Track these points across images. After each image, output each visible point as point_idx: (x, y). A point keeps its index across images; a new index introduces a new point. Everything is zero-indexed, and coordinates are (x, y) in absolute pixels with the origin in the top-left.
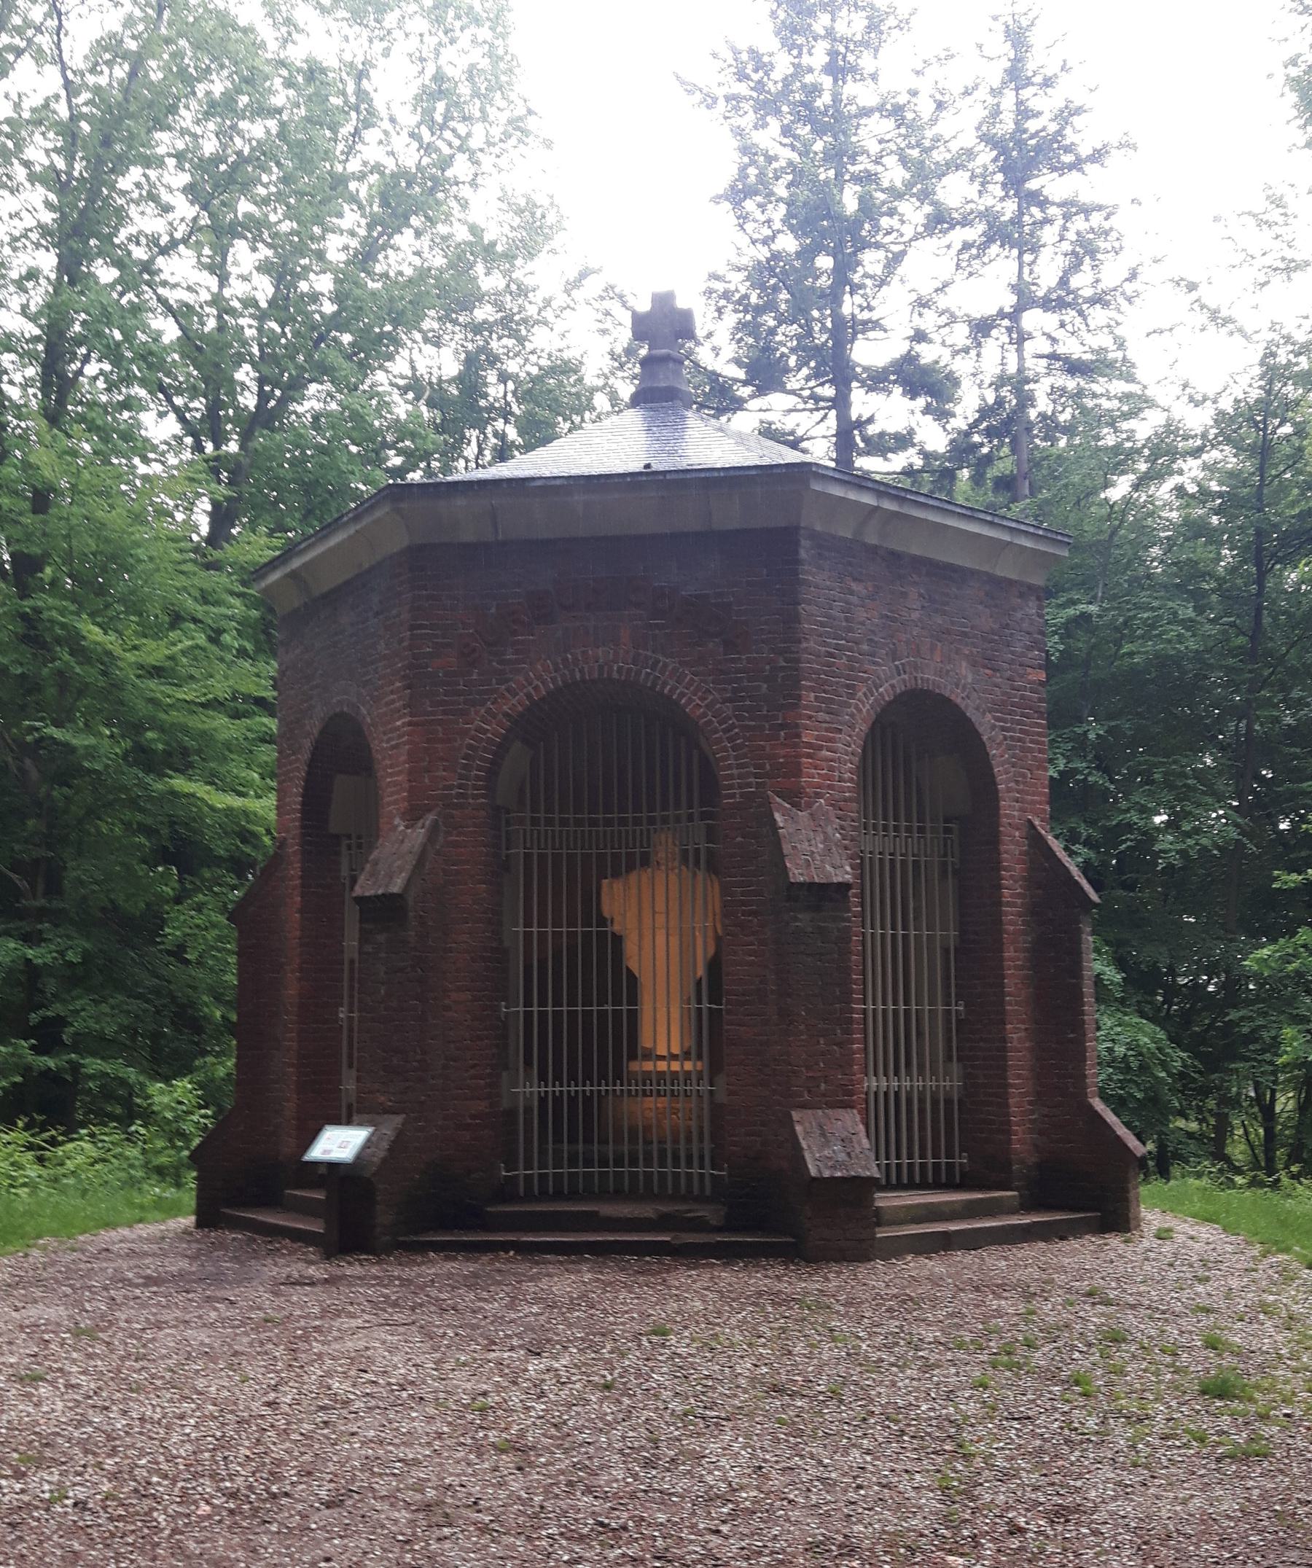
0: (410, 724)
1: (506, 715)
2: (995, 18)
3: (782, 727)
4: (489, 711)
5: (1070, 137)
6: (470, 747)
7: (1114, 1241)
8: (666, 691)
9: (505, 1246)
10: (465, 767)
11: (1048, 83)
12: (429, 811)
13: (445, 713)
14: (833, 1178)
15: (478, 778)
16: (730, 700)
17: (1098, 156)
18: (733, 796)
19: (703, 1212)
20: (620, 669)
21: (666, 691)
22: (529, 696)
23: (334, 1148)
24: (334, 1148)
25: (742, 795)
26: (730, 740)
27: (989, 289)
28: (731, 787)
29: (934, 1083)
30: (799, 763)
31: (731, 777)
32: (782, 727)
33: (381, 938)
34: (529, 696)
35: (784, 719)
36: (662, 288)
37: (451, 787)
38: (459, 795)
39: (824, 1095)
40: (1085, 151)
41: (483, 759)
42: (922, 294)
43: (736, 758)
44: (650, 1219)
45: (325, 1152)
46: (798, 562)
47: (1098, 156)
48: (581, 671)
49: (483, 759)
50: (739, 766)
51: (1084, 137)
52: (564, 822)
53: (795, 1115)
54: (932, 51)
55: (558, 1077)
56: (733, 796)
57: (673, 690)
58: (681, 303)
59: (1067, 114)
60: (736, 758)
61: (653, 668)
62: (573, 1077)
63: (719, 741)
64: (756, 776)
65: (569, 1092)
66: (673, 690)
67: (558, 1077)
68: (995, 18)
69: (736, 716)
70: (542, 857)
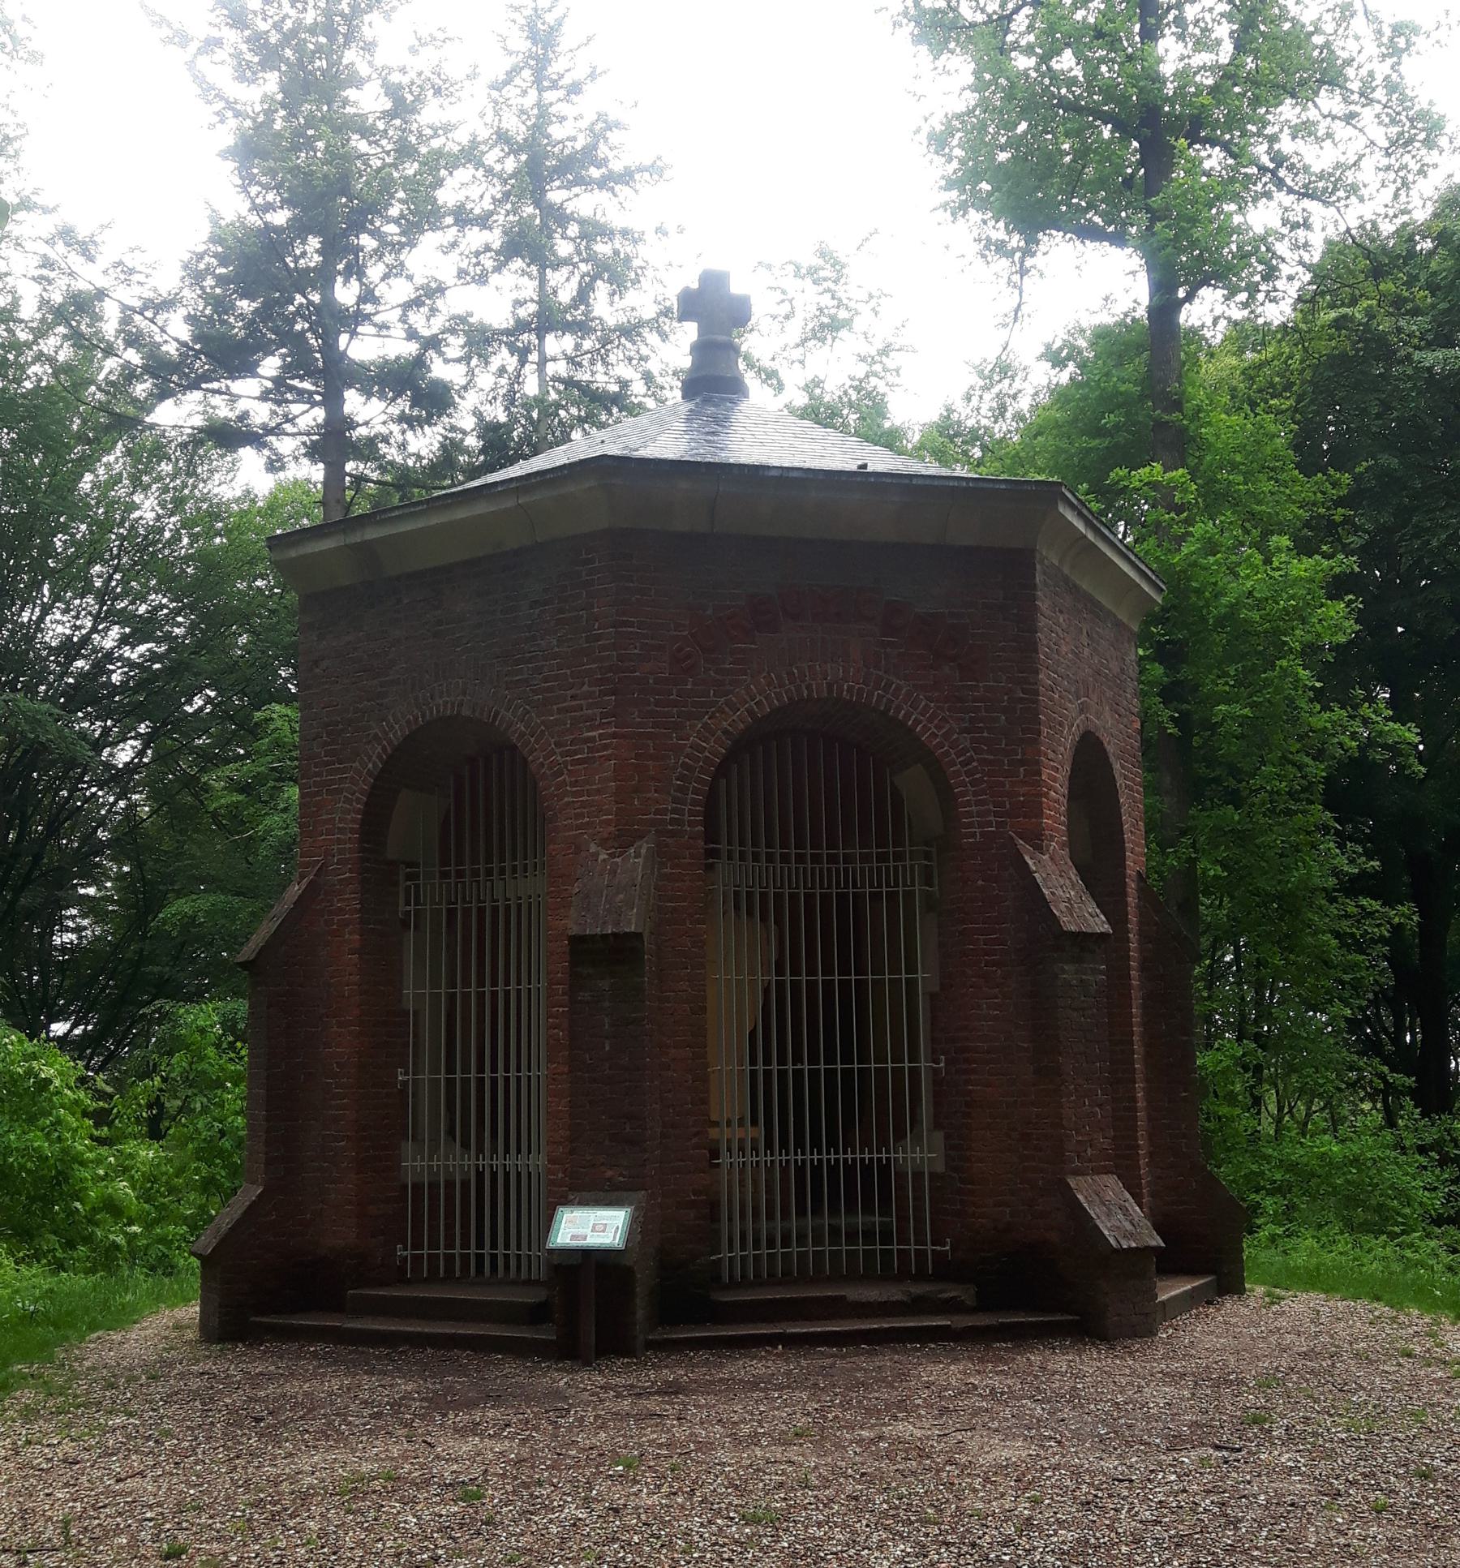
0: (614, 736)
1: (725, 732)
2: (517, 9)
3: (1022, 762)
4: (705, 726)
5: (603, 150)
6: (685, 766)
7: (1229, 1304)
8: (900, 717)
9: (771, 1340)
10: (680, 789)
11: (575, 89)
12: (641, 837)
13: (656, 725)
14: (1130, 1249)
15: (694, 803)
16: (967, 731)
17: (626, 177)
18: (973, 835)
19: (951, 1292)
20: (850, 689)
21: (900, 717)
22: (750, 712)
23: (588, 1231)
24: (588, 1231)
25: (982, 834)
26: (969, 774)
27: (499, 300)
28: (970, 825)
29: (466, 1162)
30: (1041, 803)
31: (969, 814)
32: (1022, 762)
33: (605, 984)
34: (750, 712)
35: (1024, 754)
36: (716, 265)
37: (664, 812)
38: (673, 821)
39: (1090, 1161)
40: (617, 166)
41: (699, 781)
42: (434, 293)
43: (975, 794)
44: (902, 1303)
45: (573, 1237)
46: (1034, 587)
47: (626, 177)
48: (809, 687)
49: (699, 781)
50: (978, 803)
51: (621, 153)
52: (816, 859)
53: (1072, 1182)
54: (440, 27)
55: (799, 1144)
56: (973, 835)
57: (908, 716)
58: (736, 288)
59: (601, 129)
60: (975, 794)
61: (886, 689)
62: (832, 1143)
63: (957, 774)
64: (996, 814)
65: (880, 1160)
66: (908, 716)
67: (799, 1144)
68: (517, 9)
69: (974, 749)
70: (809, 897)
